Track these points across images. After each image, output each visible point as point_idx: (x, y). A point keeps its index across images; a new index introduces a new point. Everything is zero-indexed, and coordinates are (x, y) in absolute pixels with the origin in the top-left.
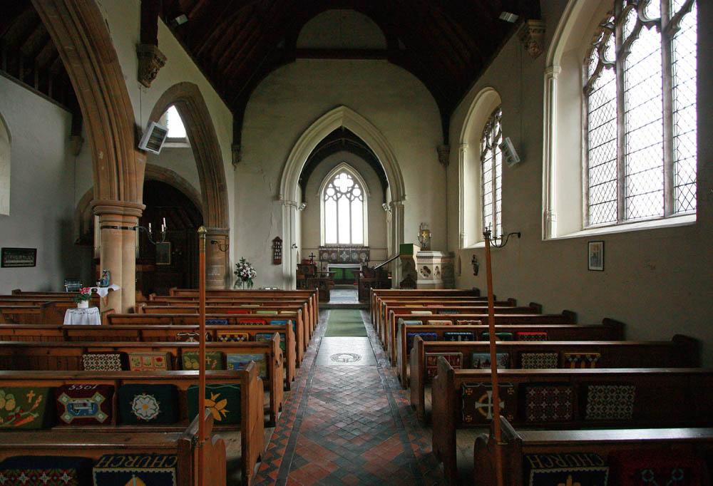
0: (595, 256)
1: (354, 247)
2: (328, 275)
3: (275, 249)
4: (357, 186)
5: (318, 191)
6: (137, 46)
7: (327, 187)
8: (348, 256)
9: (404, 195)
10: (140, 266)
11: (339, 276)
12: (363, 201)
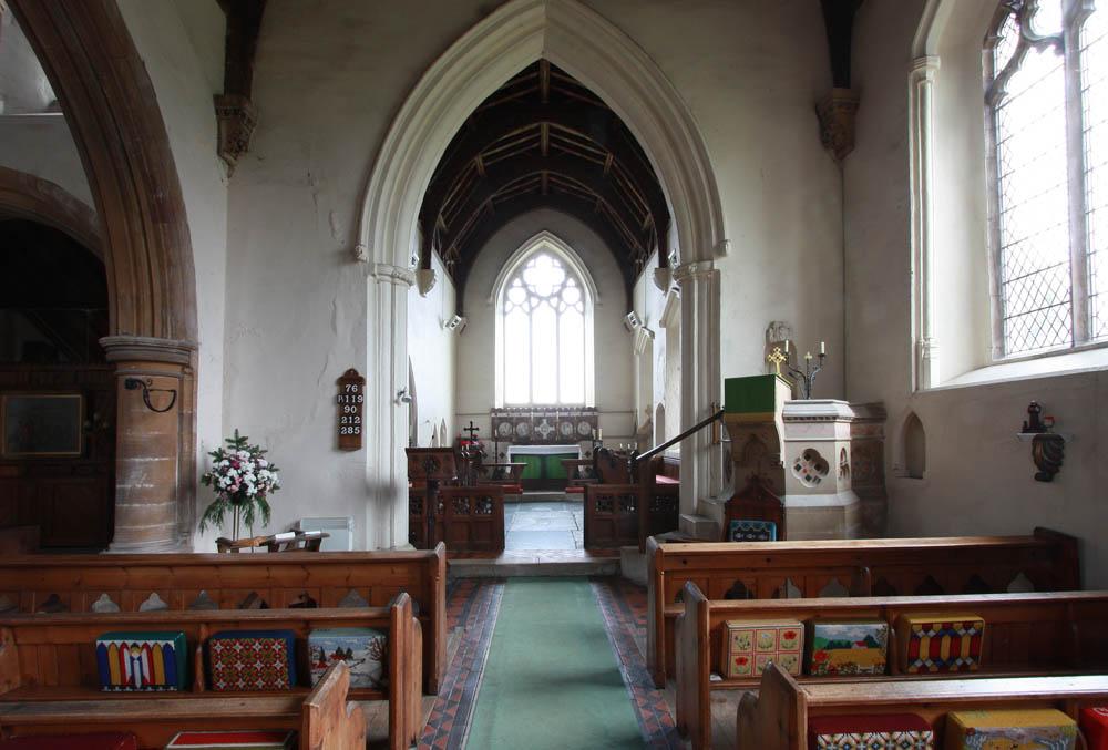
1: (566, 410)
2: (508, 470)
3: (342, 404)
4: (571, 282)
5: (489, 291)
6: (217, 99)
7: (509, 285)
8: (553, 429)
9: (722, 242)
10: (856, 426)
11: (532, 472)
12: (583, 314)
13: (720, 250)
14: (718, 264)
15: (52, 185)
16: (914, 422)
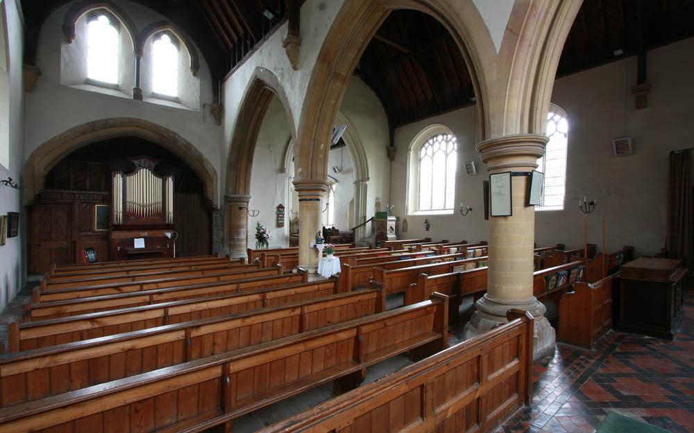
0: (350, 247)
13: (368, 179)
14: (367, 183)
15: (175, 134)
16: (405, 221)
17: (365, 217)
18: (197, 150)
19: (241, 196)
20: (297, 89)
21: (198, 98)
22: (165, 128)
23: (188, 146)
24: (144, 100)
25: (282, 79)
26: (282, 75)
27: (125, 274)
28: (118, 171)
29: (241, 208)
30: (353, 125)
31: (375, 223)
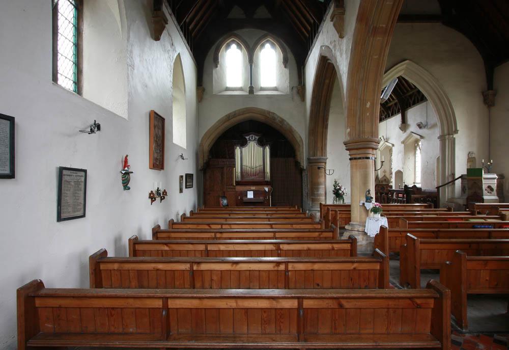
14: (455, 136)
17: (453, 175)
18: (288, 124)
19: (318, 157)
20: (344, 56)
21: (288, 84)
22: (267, 111)
23: (282, 121)
24: (255, 94)
25: (335, 50)
26: (335, 46)
27: (265, 216)
28: (237, 144)
29: (319, 168)
30: (433, 76)
31: (466, 182)
